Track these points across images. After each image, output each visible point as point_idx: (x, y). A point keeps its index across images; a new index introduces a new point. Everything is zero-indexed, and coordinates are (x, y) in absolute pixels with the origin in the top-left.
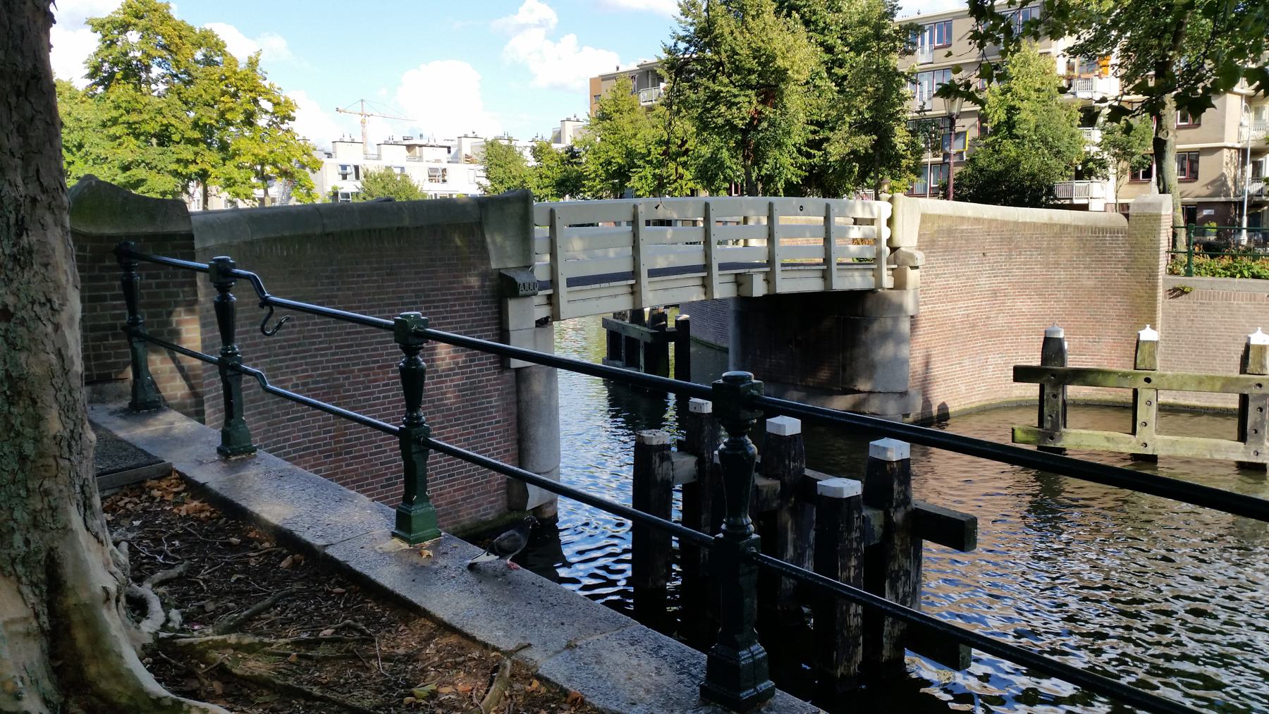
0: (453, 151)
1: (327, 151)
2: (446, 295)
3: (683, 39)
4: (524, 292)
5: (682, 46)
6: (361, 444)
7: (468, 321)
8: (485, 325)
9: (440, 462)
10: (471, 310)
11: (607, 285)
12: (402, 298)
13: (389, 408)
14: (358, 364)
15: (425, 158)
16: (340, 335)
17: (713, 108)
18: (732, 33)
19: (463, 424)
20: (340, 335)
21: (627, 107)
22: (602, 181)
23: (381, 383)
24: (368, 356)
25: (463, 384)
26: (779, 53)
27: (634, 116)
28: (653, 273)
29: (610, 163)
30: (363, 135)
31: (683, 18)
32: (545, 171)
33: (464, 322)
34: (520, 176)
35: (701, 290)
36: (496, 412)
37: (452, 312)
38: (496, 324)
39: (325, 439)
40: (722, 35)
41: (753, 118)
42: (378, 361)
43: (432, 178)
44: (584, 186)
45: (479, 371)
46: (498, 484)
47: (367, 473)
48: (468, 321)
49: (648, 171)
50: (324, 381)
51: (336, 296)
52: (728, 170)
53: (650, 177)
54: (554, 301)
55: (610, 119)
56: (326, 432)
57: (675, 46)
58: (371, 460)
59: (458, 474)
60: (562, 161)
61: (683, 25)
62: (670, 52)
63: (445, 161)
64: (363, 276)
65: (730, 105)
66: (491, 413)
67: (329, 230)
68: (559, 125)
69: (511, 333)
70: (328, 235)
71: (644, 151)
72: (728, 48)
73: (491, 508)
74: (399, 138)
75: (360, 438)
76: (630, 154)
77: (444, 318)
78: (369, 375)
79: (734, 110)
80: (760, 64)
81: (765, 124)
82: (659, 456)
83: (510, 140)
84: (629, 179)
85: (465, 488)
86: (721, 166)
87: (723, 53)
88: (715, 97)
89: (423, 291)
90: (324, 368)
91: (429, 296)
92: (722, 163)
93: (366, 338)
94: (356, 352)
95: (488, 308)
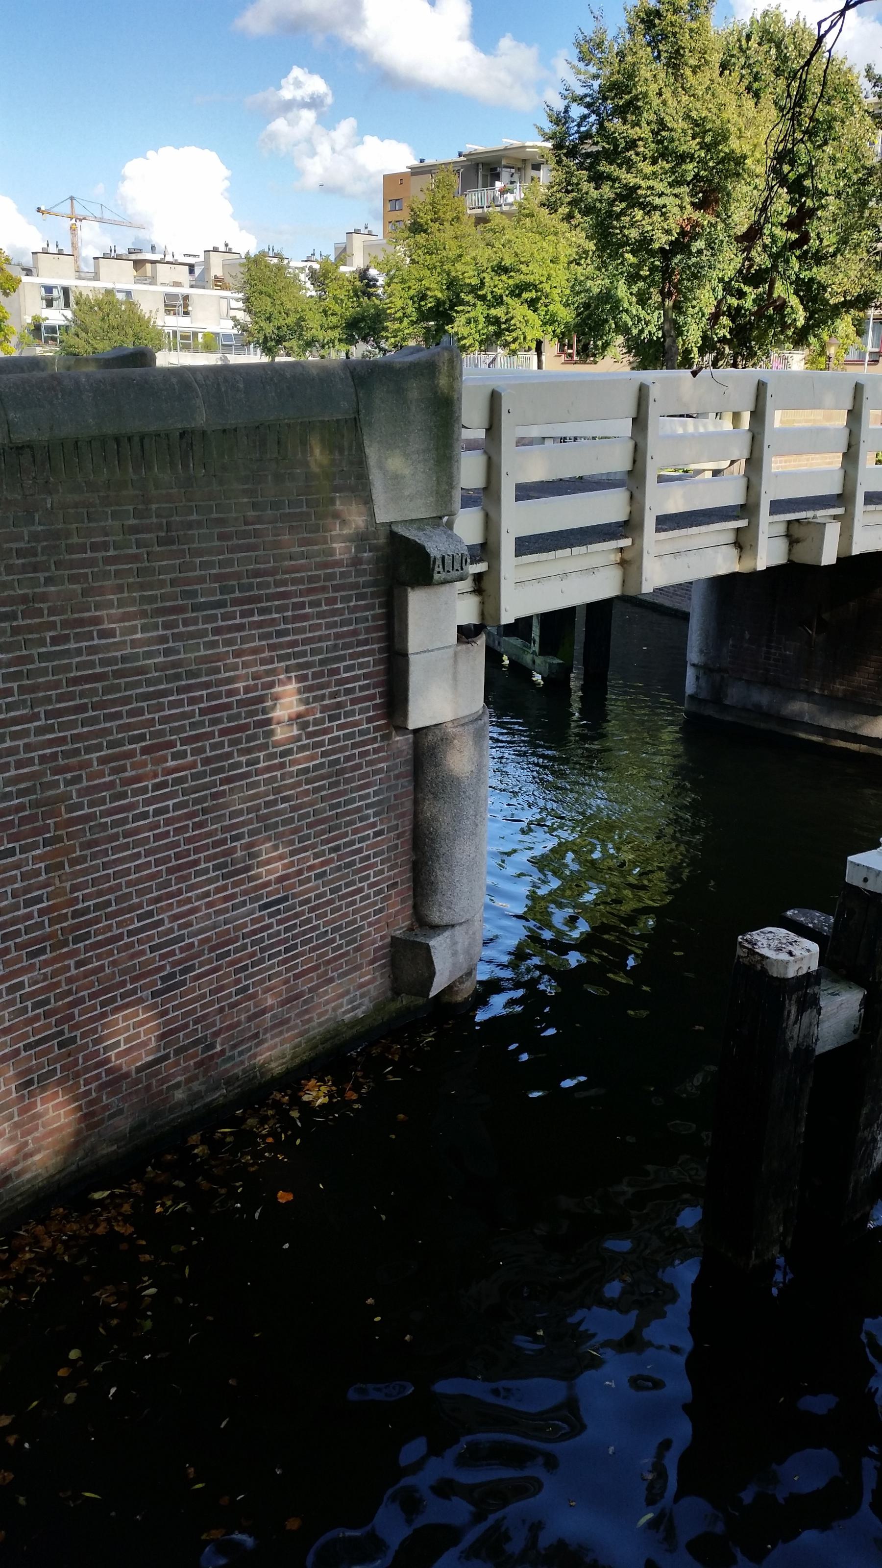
0: (198, 271)
1: (26, 266)
2: (284, 583)
3: (579, 99)
4: (443, 575)
5: (577, 111)
6: (108, 917)
7: (327, 638)
8: (360, 643)
9: (269, 926)
10: (334, 612)
11: (583, 549)
12: (193, 594)
13: (166, 834)
14: (98, 747)
15: (160, 280)
16: (56, 685)
17: (623, 213)
18: (660, 94)
19: (313, 846)
20: (56, 685)
21: (449, 216)
22: (412, 323)
23: (150, 784)
24: (121, 728)
25: (316, 768)
26: (733, 129)
27: (460, 229)
28: (666, 522)
29: (424, 297)
30: (74, 245)
31: (581, 65)
32: (329, 302)
33: (320, 639)
34: (296, 312)
35: (734, 552)
36: (376, 815)
37: (296, 619)
38: (379, 640)
39: (29, 916)
40: (645, 95)
41: (683, 233)
42: (142, 738)
43: (170, 309)
44: (385, 329)
45: (347, 737)
46: (376, 950)
47: (122, 973)
48: (327, 638)
49: (480, 311)
50: (21, 793)
51: (44, 598)
52: (624, 315)
53: (482, 319)
54: (486, 584)
55: (425, 231)
56: (28, 903)
57: (566, 111)
58: (131, 945)
59: (304, 943)
60: (355, 291)
61: (582, 77)
62: (557, 121)
63: (187, 284)
64: (105, 546)
65: (648, 208)
66: (367, 817)
67: (19, 438)
68: (343, 239)
69: (412, 658)
70: (19, 449)
71: (475, 281)
72: (653, 117)
73: (362, 996)
74: (122, 251)
75: (108, 903)
76: (452, 284)
77: (280, 634)
78: (123, 769)
79: (656, 216)
80: (703, 146)
81: (700, 244)
82: (798, 1002)
83: (282, 259)
84: (451, 321)
85: (315, 968)
86: (616, 306)
87: (644, 125)
88: (629, 195)
89: (237, 576)
90: (19, 765)
91: (250, 587)
92: (619, 301)
93: (116, 688)
94: (94, 721)
95: (367, 608)
